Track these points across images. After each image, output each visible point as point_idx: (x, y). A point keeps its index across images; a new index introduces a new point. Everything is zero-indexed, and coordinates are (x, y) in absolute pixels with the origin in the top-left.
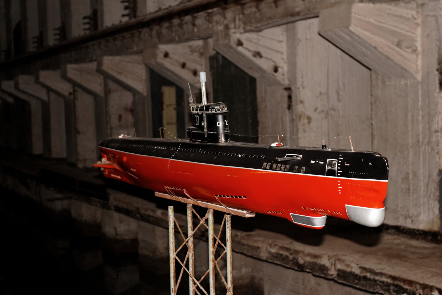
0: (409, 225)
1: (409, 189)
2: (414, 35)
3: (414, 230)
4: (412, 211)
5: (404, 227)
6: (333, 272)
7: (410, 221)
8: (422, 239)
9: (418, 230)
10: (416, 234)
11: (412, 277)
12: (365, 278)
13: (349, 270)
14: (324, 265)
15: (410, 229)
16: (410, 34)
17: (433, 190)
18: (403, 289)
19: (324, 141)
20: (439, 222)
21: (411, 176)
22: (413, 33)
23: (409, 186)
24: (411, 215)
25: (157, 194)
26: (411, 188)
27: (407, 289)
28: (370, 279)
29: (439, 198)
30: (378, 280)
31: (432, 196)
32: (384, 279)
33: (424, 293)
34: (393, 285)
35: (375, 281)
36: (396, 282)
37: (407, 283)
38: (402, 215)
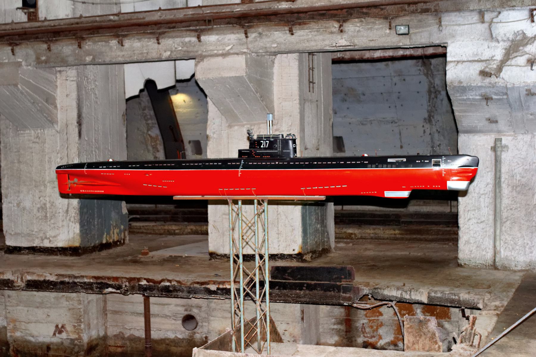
0: (47, 244)
1: (46, 216)
2: (55, 95)
3: (52, 248)
4: (50, 233)
5: (40, 247)
6: (20, 283)
7: (48, 241)
8: (60, 254)
9: (57, 248)
10: (54, 251)
11: (115, 275)
12: (62, 283)
13: (42, 279)
14: (9, 280)
15: (47, 248)
16: (53, 93)
17: (73, 215)
18: (107, 284)
19: (229, 164)
20: (80, 239)
21: (48, 205)
22: (54, 93)
23: (46, 214)
24: (48, 237)
25: (177, 197)
26: (48, 215)
27: (112, 284)
28: (68, 283)
29: (80, 221)
30: (78, 282)
31: (72, 219)
32: (86, 280)
33: (130, 285)
34: (97, 283)
35: (75, 283)
36: (99, 281)
37: (112, 280)
38: (38, 238)
